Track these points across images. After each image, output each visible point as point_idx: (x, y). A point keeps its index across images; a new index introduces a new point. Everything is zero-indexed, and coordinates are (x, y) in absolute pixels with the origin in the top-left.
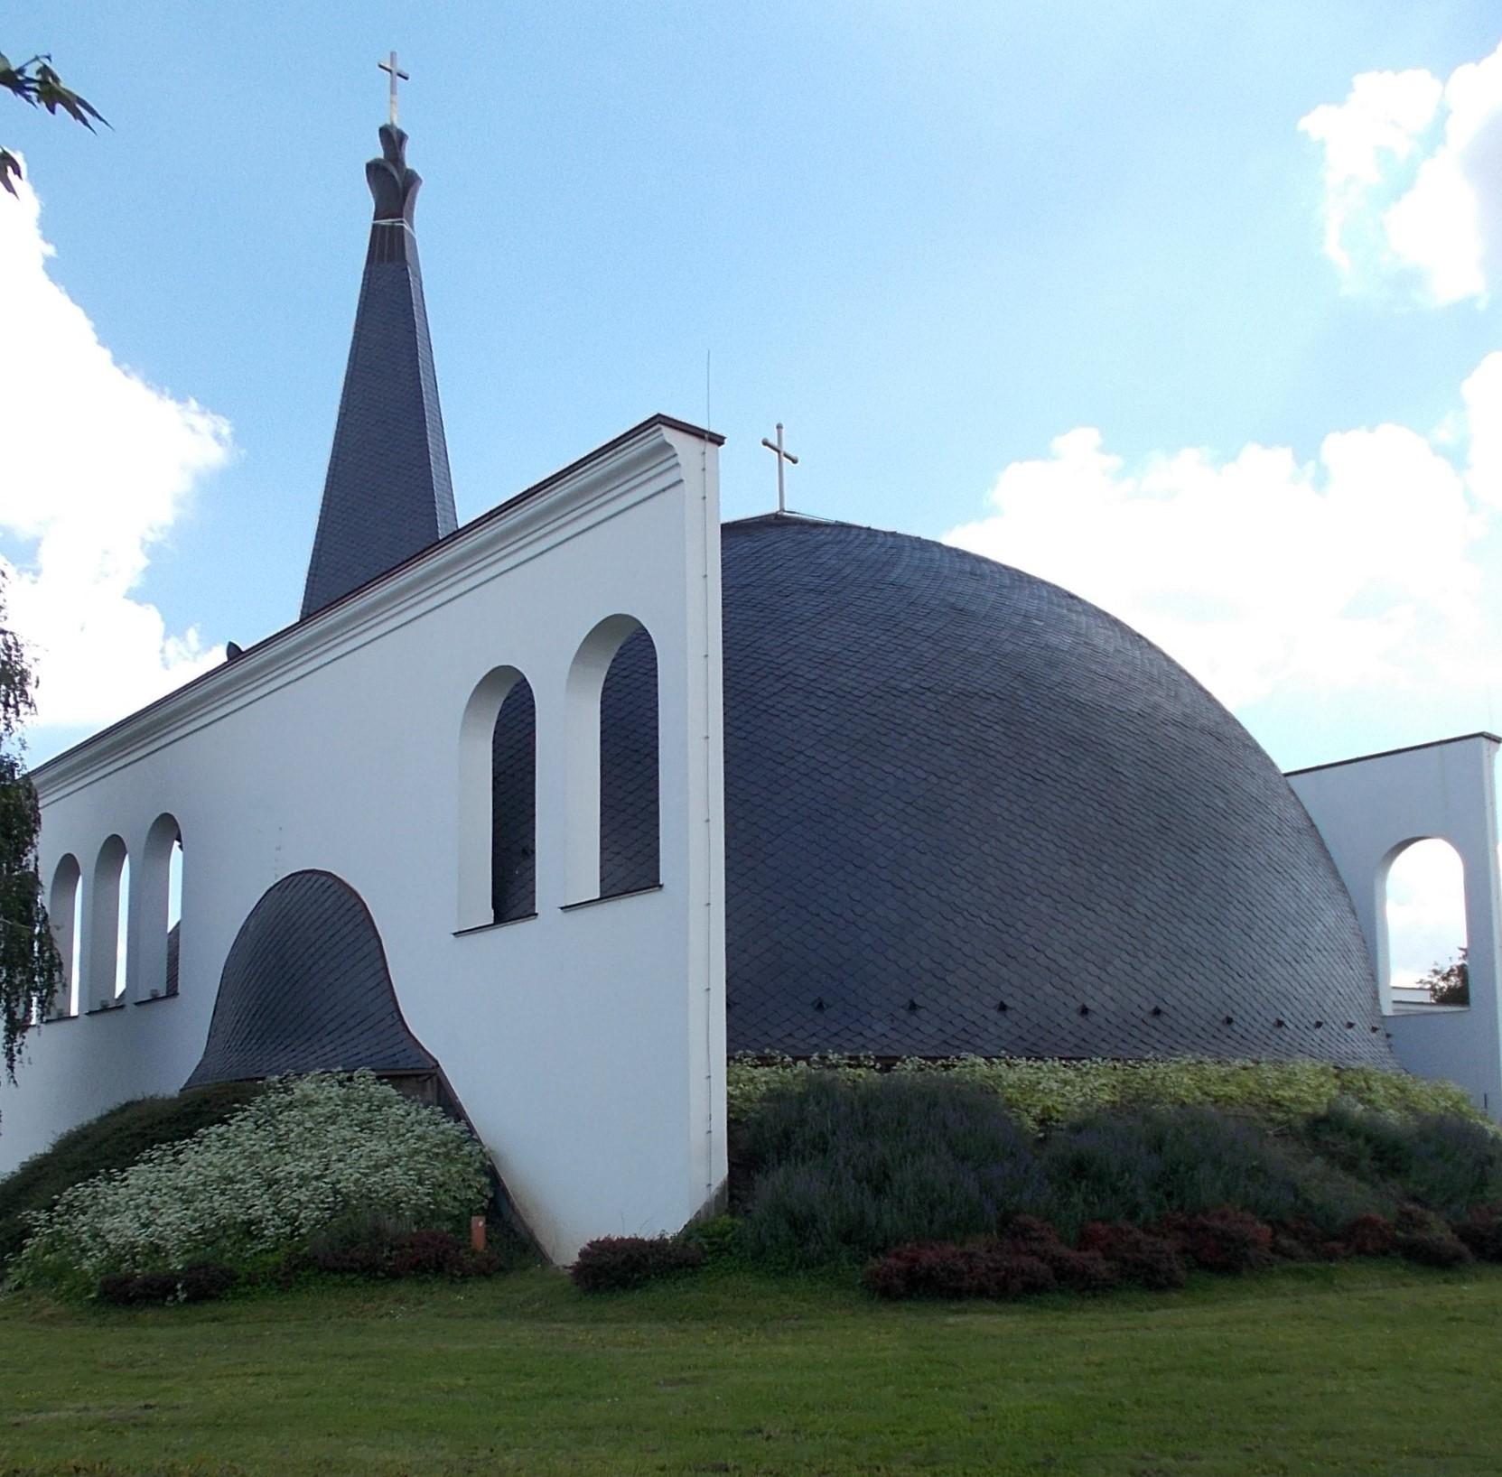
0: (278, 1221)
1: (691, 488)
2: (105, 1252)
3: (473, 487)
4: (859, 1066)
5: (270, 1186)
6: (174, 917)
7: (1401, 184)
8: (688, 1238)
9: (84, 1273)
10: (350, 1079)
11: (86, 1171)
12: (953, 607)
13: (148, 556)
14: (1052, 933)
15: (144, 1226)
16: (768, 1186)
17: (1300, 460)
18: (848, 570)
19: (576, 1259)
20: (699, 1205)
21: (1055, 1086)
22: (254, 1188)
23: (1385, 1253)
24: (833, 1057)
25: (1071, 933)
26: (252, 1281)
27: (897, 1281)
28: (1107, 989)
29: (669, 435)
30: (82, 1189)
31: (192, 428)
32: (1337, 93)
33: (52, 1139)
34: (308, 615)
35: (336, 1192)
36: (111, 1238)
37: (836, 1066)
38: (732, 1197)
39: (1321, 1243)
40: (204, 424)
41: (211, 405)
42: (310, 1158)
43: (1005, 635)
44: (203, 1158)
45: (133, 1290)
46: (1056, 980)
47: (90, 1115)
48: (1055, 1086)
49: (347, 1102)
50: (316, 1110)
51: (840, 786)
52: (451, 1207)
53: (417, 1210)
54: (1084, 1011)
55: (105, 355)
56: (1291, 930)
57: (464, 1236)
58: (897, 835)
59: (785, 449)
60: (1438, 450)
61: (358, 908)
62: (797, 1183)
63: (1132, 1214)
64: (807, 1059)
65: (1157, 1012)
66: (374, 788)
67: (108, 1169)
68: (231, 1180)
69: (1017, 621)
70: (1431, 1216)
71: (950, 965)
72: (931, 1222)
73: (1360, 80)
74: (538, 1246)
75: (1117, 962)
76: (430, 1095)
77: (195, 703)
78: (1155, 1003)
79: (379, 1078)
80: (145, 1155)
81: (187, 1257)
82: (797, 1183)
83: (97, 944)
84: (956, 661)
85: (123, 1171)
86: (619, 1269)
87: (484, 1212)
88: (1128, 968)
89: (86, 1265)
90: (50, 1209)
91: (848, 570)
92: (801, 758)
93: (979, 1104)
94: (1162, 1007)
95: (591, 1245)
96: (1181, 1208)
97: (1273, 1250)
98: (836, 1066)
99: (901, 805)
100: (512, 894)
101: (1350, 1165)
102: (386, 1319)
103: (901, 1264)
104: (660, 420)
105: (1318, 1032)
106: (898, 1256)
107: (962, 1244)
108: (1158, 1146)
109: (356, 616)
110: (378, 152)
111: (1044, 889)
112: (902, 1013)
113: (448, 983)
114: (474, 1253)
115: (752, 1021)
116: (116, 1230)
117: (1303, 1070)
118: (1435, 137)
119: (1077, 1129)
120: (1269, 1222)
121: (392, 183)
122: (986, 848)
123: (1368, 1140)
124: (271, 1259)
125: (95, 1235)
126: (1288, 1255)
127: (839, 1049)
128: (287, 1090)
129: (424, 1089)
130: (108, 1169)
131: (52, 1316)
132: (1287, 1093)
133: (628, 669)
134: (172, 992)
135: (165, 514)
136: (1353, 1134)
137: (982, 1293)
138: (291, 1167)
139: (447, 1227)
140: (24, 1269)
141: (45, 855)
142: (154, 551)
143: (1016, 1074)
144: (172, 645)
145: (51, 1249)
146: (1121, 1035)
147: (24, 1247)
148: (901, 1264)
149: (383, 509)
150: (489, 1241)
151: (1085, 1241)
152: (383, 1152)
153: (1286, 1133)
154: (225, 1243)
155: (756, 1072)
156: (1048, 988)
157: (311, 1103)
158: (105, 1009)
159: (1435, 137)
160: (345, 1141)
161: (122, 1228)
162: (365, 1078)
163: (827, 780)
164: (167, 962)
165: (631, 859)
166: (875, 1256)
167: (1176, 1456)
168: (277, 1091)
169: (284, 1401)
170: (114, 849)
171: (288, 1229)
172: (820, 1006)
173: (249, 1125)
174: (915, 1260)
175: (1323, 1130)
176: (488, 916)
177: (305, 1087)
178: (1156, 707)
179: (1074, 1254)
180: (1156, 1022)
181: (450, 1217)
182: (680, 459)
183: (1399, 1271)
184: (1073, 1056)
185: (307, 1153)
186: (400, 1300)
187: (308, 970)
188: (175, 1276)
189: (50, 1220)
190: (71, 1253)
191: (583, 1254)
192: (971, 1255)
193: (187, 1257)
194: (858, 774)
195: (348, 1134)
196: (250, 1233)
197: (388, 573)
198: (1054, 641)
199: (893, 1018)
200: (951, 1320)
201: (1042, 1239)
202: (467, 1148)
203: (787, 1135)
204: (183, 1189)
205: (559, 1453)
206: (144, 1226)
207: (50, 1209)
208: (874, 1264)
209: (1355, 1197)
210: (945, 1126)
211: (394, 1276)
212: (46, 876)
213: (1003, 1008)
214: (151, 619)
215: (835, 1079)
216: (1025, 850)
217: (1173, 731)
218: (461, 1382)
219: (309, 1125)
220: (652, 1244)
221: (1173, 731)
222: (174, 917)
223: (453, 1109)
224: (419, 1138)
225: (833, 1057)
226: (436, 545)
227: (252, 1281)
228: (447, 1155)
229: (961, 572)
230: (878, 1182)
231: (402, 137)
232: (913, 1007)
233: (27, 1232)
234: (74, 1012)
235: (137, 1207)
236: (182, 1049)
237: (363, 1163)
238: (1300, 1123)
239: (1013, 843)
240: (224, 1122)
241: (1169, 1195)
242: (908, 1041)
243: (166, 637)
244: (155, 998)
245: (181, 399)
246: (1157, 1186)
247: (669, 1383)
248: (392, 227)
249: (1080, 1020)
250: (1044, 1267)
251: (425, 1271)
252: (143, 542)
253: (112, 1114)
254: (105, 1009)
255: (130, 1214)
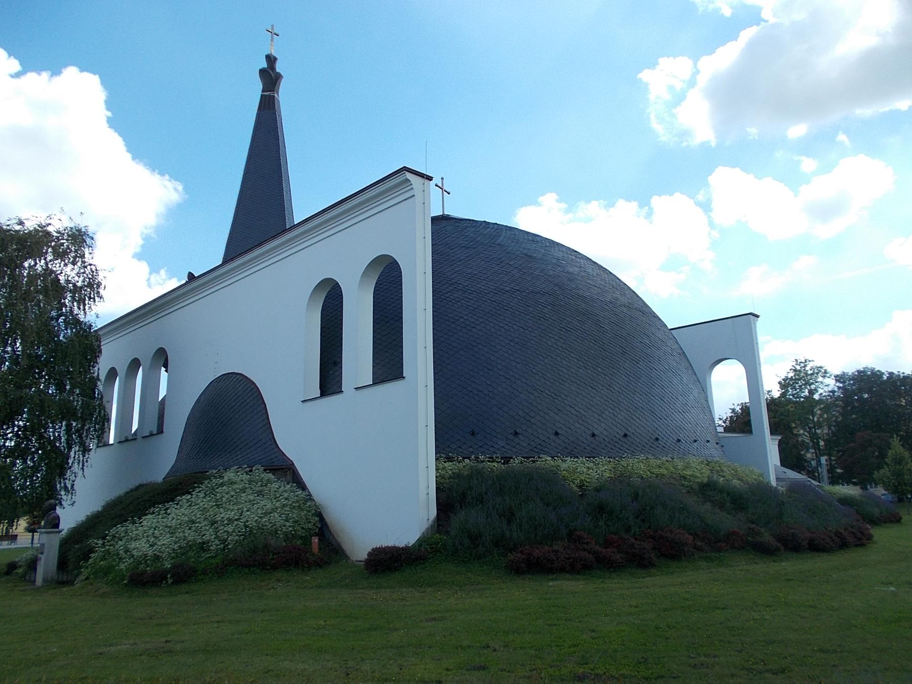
0: (217, 542)
1: (418, 199)
2: (132, 560)
3: (304, 202)
4: (493, 462)
5: (212, 525)
6: (163, 393)
7: (679, 99)
8: (420, 546)
9: (121, 570)
10: (251, 471)
11: (122, 519)
12: (526, 255)
13: (144, 239)
14: (578, 400)
15: (151, 546)
16: (458, 519)
17: (641, 206)
18: (479, 239)
19: (366, 557)
20: (423, 530)
21: (585, 470)
22: (205, 526)
23: (743, 548)
24: (481, 457)
25: (586, 399)
26: (204, 572)
27: (522, 565)
28: (603, 425)
29: (409, 176)
30: (120, 529)
31: (165, 187)
32: (653, 65)
33: (103, 503)
34: (226, 261)
35: (246, 527)
36: (135, 553)
37: (482, 462)
38: (438, 526)
39: (716, 544)
40: (170, 185)
41: (175, 177)
42: (232, 510)
43: (550, 267)
44: (179, 511)
45: (146, 579)
46: (580, 421)
47: (120, 491)
48: (585, 470)
49: (250, 482)
50: (236, 486)
51: (480, 333)
52: (301, 533)
53: (286, 534)
54: (593, 435)
55: (129, 156)
56: (680, 398)
57: (307, 547)
58: (506, 355)
59: (445, 188)
60: (698, 204)
61: (255, 390)
62: (468, 517)
63: (628, 530)
64: (468, 458)
65: (625, 435)
66: (264, 335)
67: (133, 518)
68: (193, 522)
69: (554, 261)
70: (763, 530)
71: (532, 414)
72: (536, 535)
73: (661, 60)
74: (343, 550)
75: (607, 413)
76: (289, 478)
77: (178, 297)
78: (625, 431)
79: (265, 470)
80: (151, 510)
81: (173, 561)
82: (468, 517)
83: (125, 407)
84: (529, 278)
85: (140, 518)
86: (386, 561)
87: (316, 534)
88: (612, 416)
89: (122, 566)
90: (104, 538)
91: (479, 239)
92: (462, 320)
93: (551, 478)
94: (628, 433)
95: (373, 550)
96: (649, 527)
97: (694, 548)
98: (482, 462)
99: (508, 342)
100: (330, 380)
101: (722, 506)
102: (272, 591)
103: (523, 556)
104: (405, 169)
105: (695, 444)
106: (522, 552)
107: (551, 546)
108: (636, 497)
109: (249, 261)
110: (265, 65)
111: (572, 379)
112: (511, 437)
113: (299, 426)
114: (314, 554)
115: (447, 440)
116: (137, 548)
117: (694, 462)
118: (692, 83)
119: (598, 490)
120: (691, 534)
121: (270, 77)
122: (546, 361)
123: (728, 494)
124: (213, 561)
125: (127, 551)
126: (699, 549)
127: (483, 453)
128: (221, 477)
129: (285, 476)
130: (133, 518)
131: (104, 593)
132: (689, 473)
133: (387, 279)
134: (160, 431)
135: (152, 221)
136: (721, 491)
137: (562, 570)
138: (223, 515)
139: (299, 542)
140: (89, 569)
141: (102, 367)
142: (147, 238)
143: (567, 464)
144: (153, 278)
145: (103, 558)
146: (611, 446)
147: (90, 558)
148: (523, 556)
149: (261, 215)
150: (320, 549)
151: (607, 544)
152: (269, 506)
153: (690, 491)
154: (191, 554)
155: (446, 465)
156: (577, 425)
157: (232, 483)
158: (127, 440)
159: (692, 83)
160: (250, 501)
161: (141, 547)
162: (258, 469)
163: (474, 330)
164: (159, 415)
165: (388, 364)
166: (510, 552)
167: (705, 656)
168: (215, 478)
169: (236, 636)
170: (135, 364)
171: (222, 546)
172: (473, 434)
173: (202, 495)
174: (529, 554)
175: (707, 490)
176: (317, 393)
177: (230, 475)
178: (617, 299)
179: (604, 550)
180: (624, 440)
181: (301, 538)
182: (413, 186)
183: (751, 556)
184: (591, 456)
185: (231, 507)
186: (279, 580)
187: (231, 419)
188: (167, 571)
189: (104, 544)
190: (115, 560)
191: (370, 554)
192: (557, 551)
193: (173, 561)
194: (488, 327)
195: (252, 498)
196: (203, 548)
197: (274, 237)
198: (571, 270)
199: (507, 439)
200: (551, 584)
201: (587, 543)
202: (309, 504)
203: (464, 495)
204: (170, 527)
205: (391, 662)
206: (151, 546)
207: (104, 538)
208: (511, 557)
209: (726, 522)
210: (538, 489)
211: (275, 568)
212: (102, 377)
213: (557, 434)
214: (144, 267)
215: (483, 468)
216: (564, 362)
217: (625, 310)
218: (322, 623)
219: (233, 493)
220: (403, 549)
221: (625, 310)
222: (163, 393)
223: (302, 486)
224: (286, 499)
225: (481, 457)
226: (285, 231)
227: (204, 572)
228: (299, 507)
229: (529, 240)
230: (509, 516)
231: (275, 59)
232: (516, 434)
233: (92, 550)
234: (111, 442)
235: (148, 536)
236: (165, 458)
237: (260, 512)
238: (696, 486)
239: (559, 359)
240: (189, 493)
241: (643, 521)
242: (514, 450)
243: (151, 273)
244: (152, 435)
245: (162, 174)
246: (637, 517)
247: (427, 620)
248: (269, 96)
249: (592, 439)
250: (591, 556)
251: (290, 565)
252: (142, 233)
253: (132, 491)
254: (127, 440)
255: (144, 540)
